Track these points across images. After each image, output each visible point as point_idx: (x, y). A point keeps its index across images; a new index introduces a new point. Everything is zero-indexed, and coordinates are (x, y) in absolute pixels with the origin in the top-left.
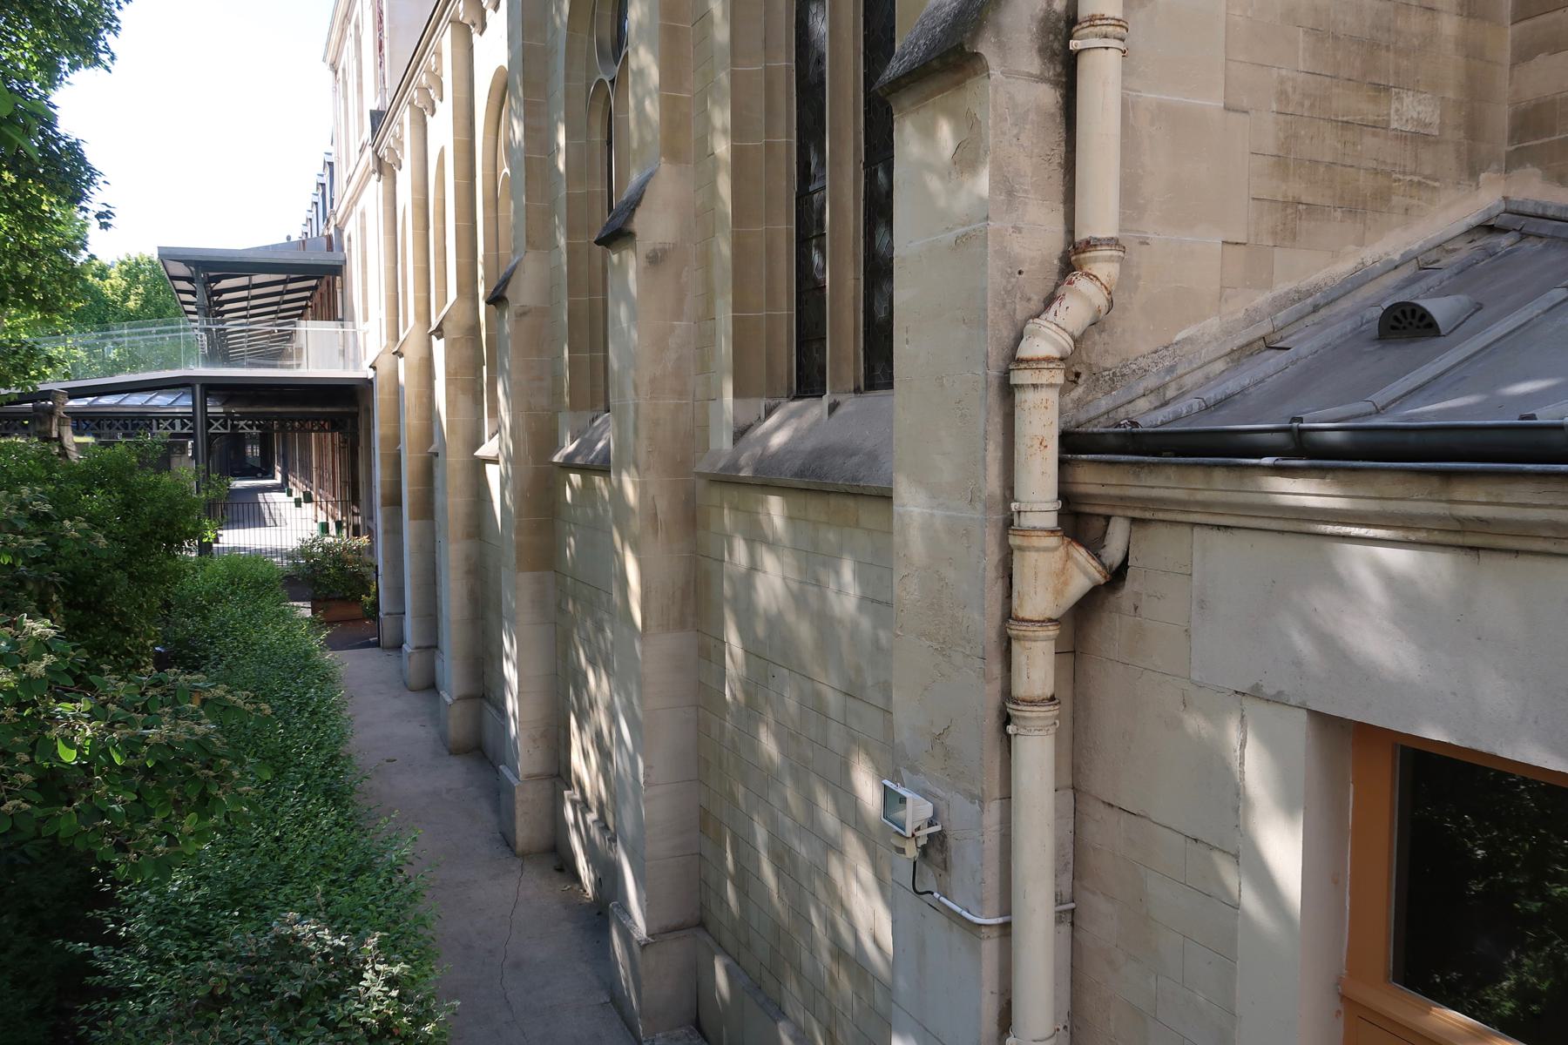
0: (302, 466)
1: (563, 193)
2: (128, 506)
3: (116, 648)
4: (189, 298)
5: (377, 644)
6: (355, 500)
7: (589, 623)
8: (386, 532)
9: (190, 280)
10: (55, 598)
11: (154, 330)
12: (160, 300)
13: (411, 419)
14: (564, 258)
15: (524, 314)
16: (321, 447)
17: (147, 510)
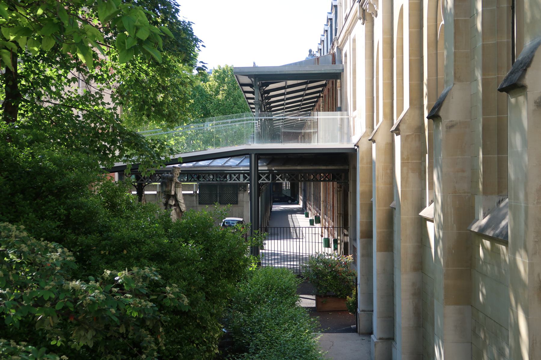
0: (314, 199)
1: (480, 44)
2: (207, 250)
3: (198, 339)
4: (251, 95)
5: (355, 331)
6: (345, 225)
7: (495, 350)
8: (363, 256)
9: (251, 85)
10: (161, 330)
11: (230, 121)
12: (236, 93)
13: (380, 185)
14: (480, 88)
15: (452, 126)
16: (326, 190)
17: (218, 253)
